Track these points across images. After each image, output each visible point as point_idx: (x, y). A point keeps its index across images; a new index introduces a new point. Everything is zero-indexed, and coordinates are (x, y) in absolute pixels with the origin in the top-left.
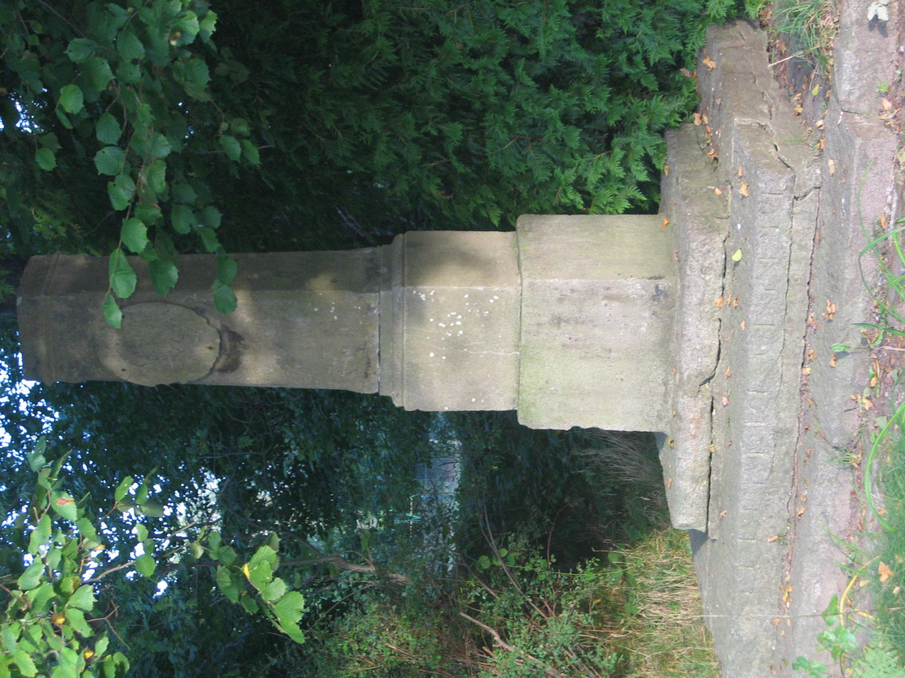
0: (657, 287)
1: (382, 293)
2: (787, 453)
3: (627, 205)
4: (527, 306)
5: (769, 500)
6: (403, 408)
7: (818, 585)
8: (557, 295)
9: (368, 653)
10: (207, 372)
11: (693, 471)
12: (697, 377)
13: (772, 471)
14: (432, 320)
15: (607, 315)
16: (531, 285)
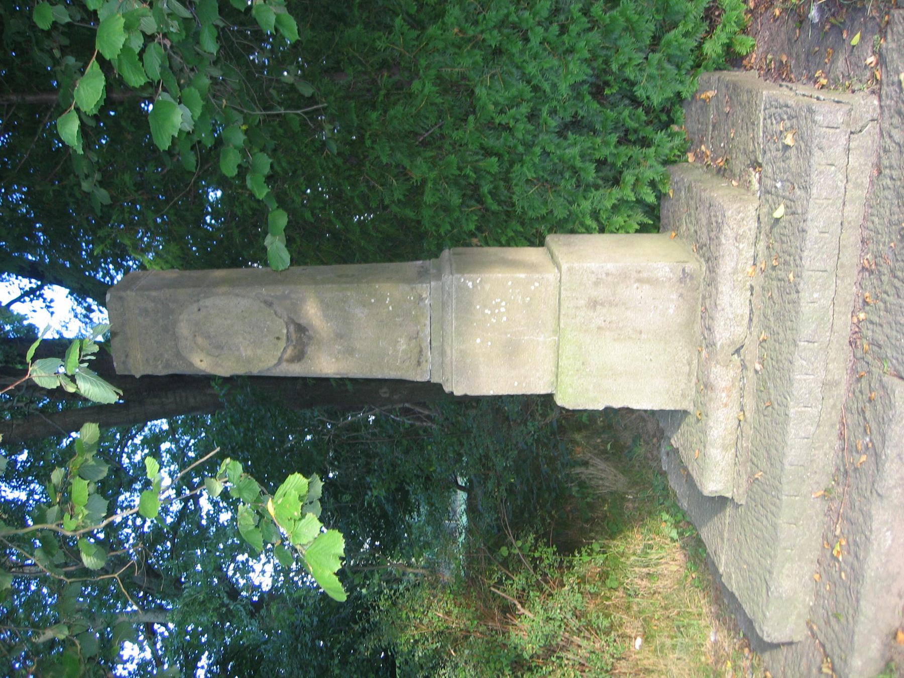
0: (684, 270)
1: (433, 283)
2: (834, 406)
3: (638, 227)
4: (566, 290)
5: (814, 455)
6: (452, 393)
7: (888, 533)
8: (593, 278)
9: (421, 620)
10: (276, 362)
11: (723, 439)
12: (729, 346)
13: (818, 426)
14: (478, 307)
15: (639, 297)
16: (570, 269)
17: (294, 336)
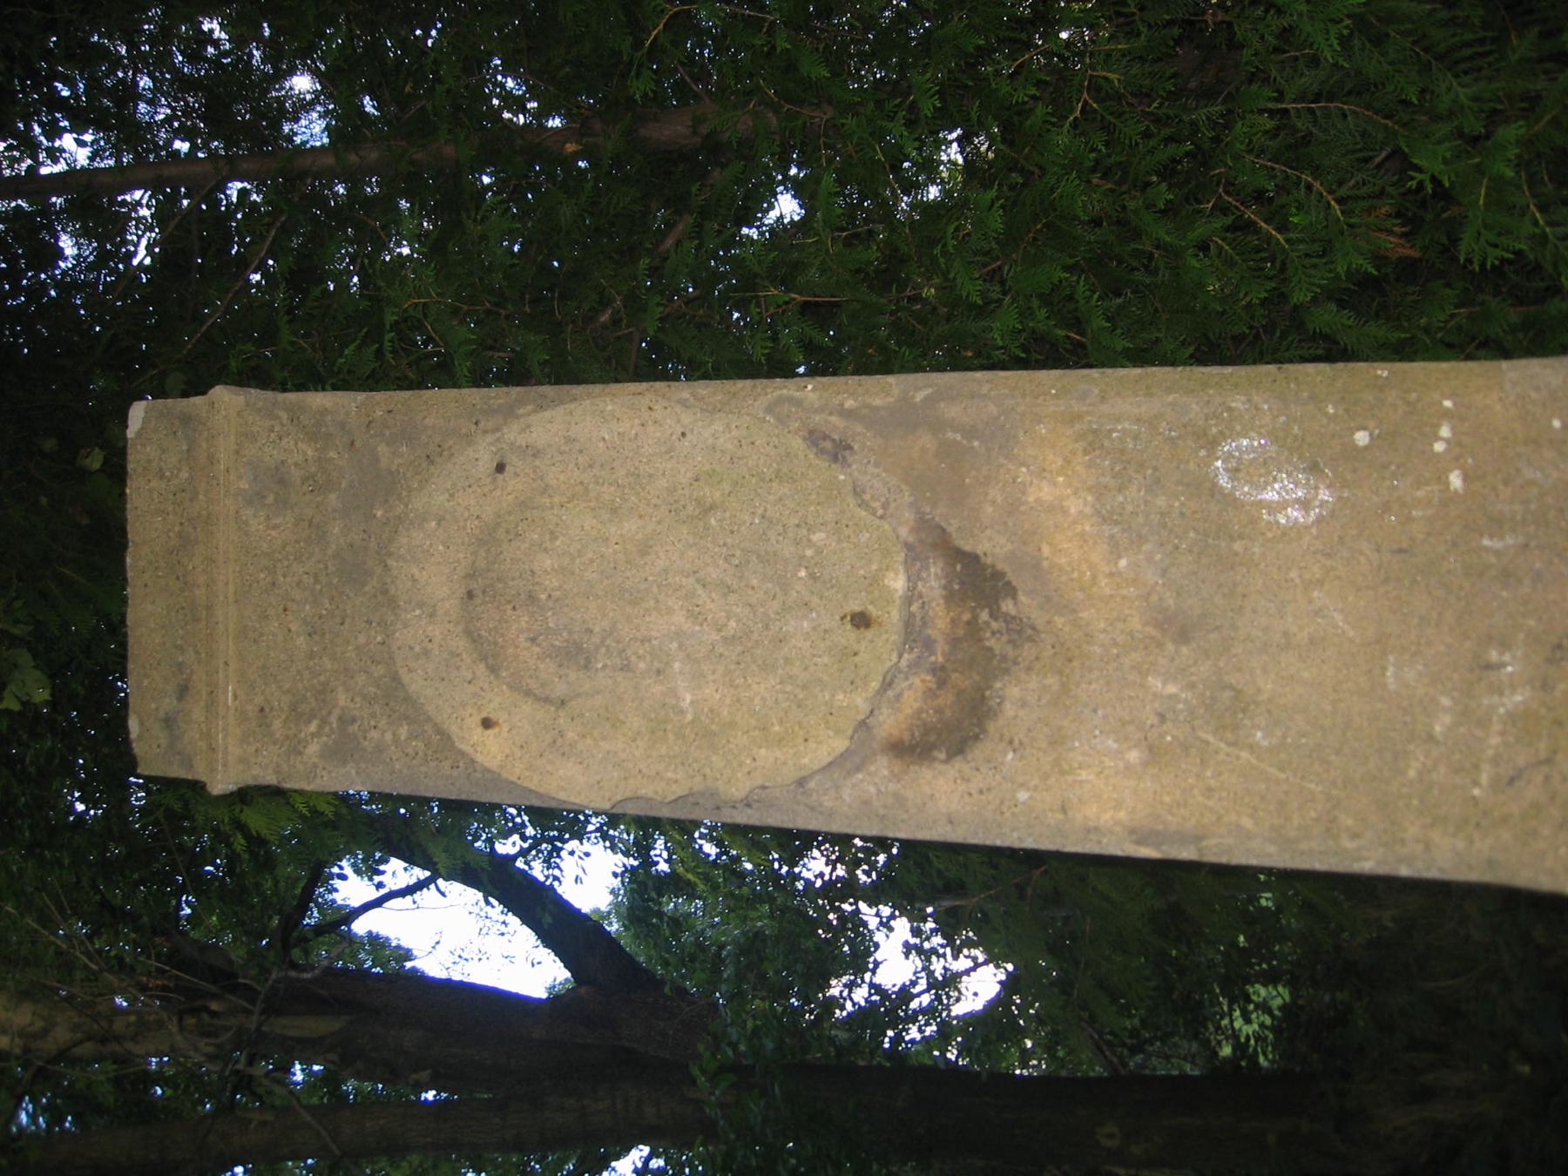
17: (940, 620)
